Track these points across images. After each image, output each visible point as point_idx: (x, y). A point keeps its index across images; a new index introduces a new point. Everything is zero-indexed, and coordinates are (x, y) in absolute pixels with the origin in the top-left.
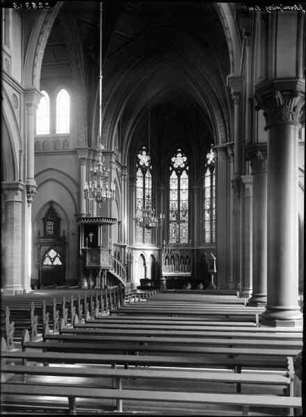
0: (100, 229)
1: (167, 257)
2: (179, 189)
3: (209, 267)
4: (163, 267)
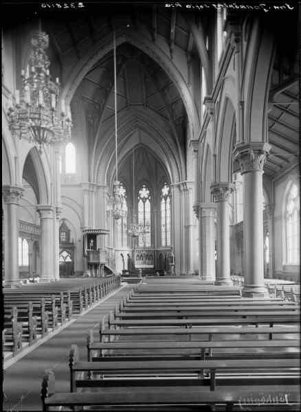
0: (98, 237)
1: (138, 256)
2: (144, 209)
3: (154, 147)
4: (136, 262)
